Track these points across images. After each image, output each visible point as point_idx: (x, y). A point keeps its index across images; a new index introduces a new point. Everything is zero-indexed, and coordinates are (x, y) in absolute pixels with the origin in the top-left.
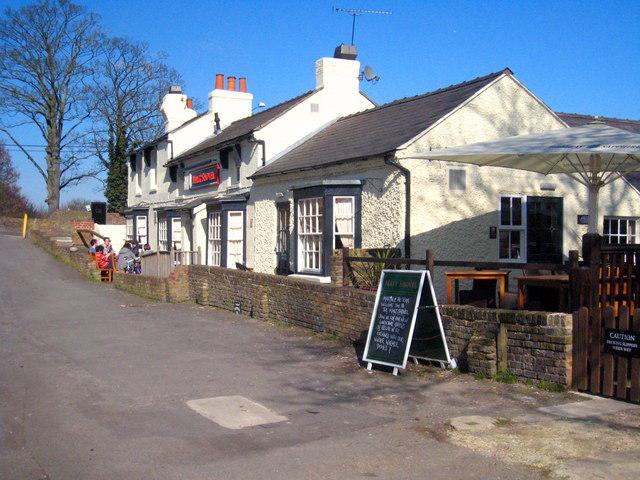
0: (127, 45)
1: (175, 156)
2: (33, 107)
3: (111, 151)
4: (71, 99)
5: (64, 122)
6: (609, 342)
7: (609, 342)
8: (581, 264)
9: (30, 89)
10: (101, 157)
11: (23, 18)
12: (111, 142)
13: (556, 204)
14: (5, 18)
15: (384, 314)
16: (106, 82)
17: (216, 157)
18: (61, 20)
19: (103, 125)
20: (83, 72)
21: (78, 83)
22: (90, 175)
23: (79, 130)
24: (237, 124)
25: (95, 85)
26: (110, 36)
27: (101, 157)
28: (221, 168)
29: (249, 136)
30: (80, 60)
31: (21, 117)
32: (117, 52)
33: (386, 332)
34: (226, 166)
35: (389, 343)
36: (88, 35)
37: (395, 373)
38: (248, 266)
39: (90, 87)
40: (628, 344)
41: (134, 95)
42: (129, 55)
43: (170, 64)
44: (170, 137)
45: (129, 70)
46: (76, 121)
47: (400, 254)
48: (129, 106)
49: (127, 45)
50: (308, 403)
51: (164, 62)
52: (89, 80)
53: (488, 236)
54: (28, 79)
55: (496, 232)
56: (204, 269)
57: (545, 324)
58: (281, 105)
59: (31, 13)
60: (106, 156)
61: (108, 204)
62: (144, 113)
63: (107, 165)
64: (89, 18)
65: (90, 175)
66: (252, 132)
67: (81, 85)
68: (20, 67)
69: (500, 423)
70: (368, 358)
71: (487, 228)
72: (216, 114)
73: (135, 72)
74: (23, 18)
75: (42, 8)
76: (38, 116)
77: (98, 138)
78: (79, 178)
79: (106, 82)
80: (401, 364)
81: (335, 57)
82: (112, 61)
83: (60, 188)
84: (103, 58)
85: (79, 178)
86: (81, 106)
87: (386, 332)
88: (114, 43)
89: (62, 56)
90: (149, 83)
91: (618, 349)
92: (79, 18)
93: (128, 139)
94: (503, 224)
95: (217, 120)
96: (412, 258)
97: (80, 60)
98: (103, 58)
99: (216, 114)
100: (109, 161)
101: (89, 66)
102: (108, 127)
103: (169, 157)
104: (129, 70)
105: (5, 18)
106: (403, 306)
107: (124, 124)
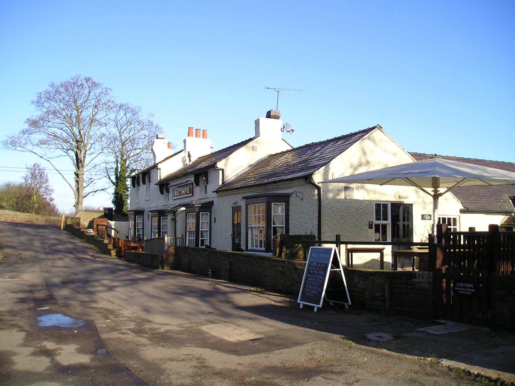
0: (128, 108)
1: (162, 178)
2: (66, 146)
3: (116, 174)
4: (92, 141)
5: (87, 156)
6: (457, 288)
7: (457, 288)
8: (464, 247)
9: (64, 135)
10: (110, 179)
11: (62, 90)
12: (117, 169)
13: (408, 209)
14: (50, 89)
15: (310, 274)
16: (115, 131)
17: (192, 179)
18: (86, 92)
19: (112, 158)
20: (100, 125)
21: (96, 131)
22: (103, 190)
23: (97, 161)
24: (202, 159)
25: (108, 133)
26: (118, 102)
27: (110, 179)
28: (195, 185)
29: (213, 166)
30: (97, 117)
31: (59, 152)
32: (122, 113)
33: (311, 284)
34: (197, 184)
35: (312, 291)
36: (103, 101)
37: (315, 310)
38: (212, 247)
39: (104, 135)
40: (469, 290)
41: (133, 141)
42: (129, 115)
43: (156, 121)
44: (159, 166)
45: (128, 124)
46: (94, 156)
47: (315, 238)
48: (128, 146)
49: (128, 108)
50: (176, 325)
51: (151, 119)
52: (103, 130)
53: (368, 227)
54: (64, 129)
55: (372, 225)
56: (188, 248)
57: (416, 278)
58: (277, 154)
59: (66, 86)
60: (113, 178)
61: (114, 209)
62: (138, 151)
63: (113, 183)
64: (104, 91)
65: (103, 190)
66: (216, 163)
67: (98, 133)
68: (58, 121)
69: (396, 338)
70: (300, 300)
71: (368, 223)
72: (189, 152)
73: (132, 126)
74: (62, 90)
75: (74, 83)
76: (70, 152)
77: (108, 166)
78: (95, 192)
79: (115, 131)
80: (319, 305)
81: (267, 117)
82: (119, 118)
83: (84, 198)
84: (112, 116)
85: (95, 192)
86: (97, 146)
87: (311, 284)
88: (120, 107)
89: (86, 114)
90: (142, 132)
91: (462, 292)
92: (98, 91)
93: (128, 167)
94: (376, 220)
95: (189, 156)
96: (322, 240)
97: (97, 117)
98: (112, 116)
99: (189, 152)
100: (115, 181)
101: (104, 121)
102: (115, 160)
103: (159, 179)
104: (128, 124)
105: (50, 89)
106: (321, 269)
107: (125, 157)
